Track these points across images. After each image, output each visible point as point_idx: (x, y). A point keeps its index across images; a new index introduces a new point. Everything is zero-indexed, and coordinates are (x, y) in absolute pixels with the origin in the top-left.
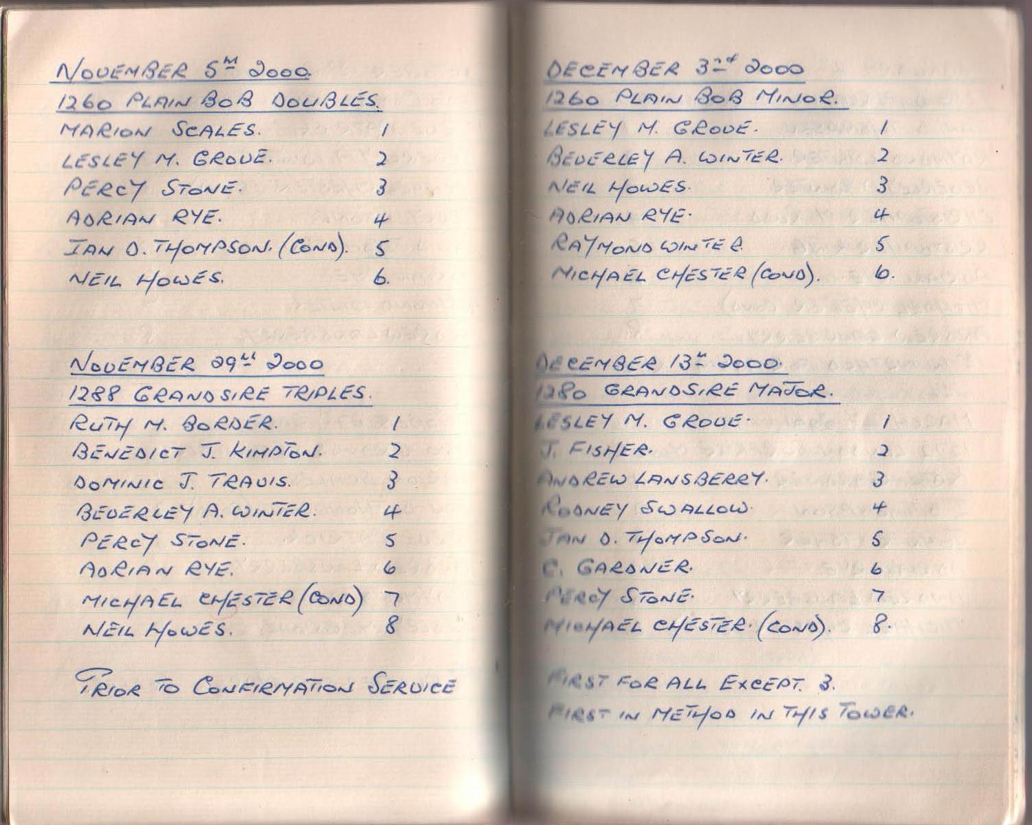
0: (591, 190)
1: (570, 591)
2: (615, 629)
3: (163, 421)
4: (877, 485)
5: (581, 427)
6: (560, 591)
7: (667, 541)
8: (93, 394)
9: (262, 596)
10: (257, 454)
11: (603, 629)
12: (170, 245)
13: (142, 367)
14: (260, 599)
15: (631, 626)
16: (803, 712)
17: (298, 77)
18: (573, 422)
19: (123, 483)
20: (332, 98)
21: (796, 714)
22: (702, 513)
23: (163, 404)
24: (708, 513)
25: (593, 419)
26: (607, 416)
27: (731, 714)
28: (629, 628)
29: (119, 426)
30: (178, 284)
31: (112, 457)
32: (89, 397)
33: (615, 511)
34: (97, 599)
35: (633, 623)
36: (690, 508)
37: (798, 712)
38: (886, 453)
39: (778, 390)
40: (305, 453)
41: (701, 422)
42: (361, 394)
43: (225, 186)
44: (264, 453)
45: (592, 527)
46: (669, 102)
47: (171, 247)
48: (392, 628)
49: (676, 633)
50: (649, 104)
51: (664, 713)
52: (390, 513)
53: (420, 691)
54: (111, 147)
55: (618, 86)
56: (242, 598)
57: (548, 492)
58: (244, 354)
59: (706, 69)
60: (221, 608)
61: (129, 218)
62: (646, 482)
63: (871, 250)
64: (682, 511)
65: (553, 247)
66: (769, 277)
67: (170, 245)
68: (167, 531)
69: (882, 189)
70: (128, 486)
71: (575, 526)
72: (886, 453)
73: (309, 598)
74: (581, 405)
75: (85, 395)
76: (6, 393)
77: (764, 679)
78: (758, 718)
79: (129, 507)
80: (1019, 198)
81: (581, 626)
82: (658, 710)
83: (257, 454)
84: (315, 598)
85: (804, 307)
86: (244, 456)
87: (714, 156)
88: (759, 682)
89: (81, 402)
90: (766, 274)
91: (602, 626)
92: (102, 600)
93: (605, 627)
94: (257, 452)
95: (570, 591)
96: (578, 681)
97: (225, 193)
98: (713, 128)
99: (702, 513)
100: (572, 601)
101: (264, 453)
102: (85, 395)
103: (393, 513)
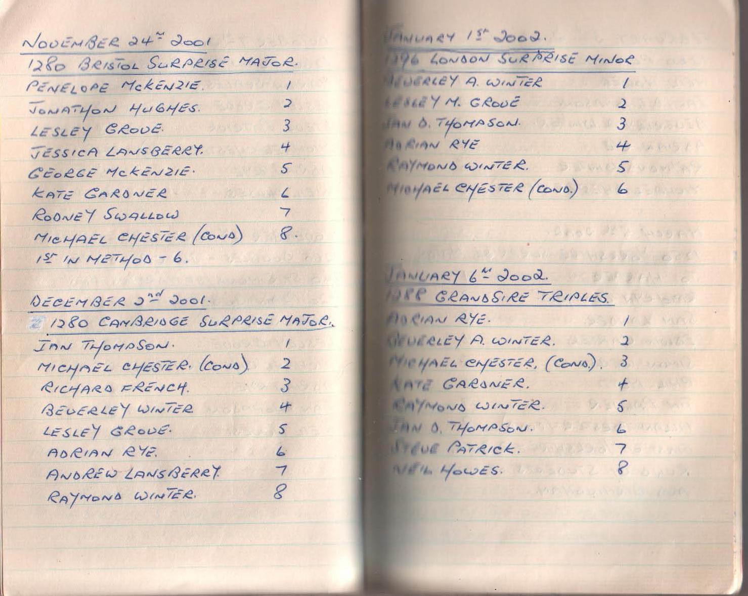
0: (34, 133)
7: (464, 125)
9: (511, 361)
11: (424, 191)
12: (460, 426)
16: (99, 346)
17: (472, 283)
18: (60, 132)
20: (87, 62)
21: (122, 260)
22: (154, 218)
23: (455, 303)
27: (108, 389)
30: (491, 86)
31: (153, 476)
33: (454, 342)
34: (48, 366)
36: (142, 474)
40: (131, 152)
41: (93, 498)
42: (623, 168)
43: (504, 383)
45: (440, 375)
50: (464, 302)
51: (95, 260)
52: (621, 146)
54: (68, 100)
56: (499, 361)
57: (395, 396)
58: (485, 268)
59: (624, 125)
60: (139, 372)
62: (133, 477)
63: (614, 409)
66: (544, 191)
67: (460, 426)
68: (109, 424)
69: (286, 128)
71: (415, 374)
73: (41, 301)
79: (497, 359)
80: (736, 188)
81: (409, 189)
82: (284, 317)
84: (206, 236)
85: (598, 405)
90: (542, 189)
91: (423, 189)
92: (52, 366)
93: (425, 189)
96: (412, 143)
97: (521, 409)
98: (57, 174)
99: (154, 218)
100: (421, 84)
103: (624, 146)
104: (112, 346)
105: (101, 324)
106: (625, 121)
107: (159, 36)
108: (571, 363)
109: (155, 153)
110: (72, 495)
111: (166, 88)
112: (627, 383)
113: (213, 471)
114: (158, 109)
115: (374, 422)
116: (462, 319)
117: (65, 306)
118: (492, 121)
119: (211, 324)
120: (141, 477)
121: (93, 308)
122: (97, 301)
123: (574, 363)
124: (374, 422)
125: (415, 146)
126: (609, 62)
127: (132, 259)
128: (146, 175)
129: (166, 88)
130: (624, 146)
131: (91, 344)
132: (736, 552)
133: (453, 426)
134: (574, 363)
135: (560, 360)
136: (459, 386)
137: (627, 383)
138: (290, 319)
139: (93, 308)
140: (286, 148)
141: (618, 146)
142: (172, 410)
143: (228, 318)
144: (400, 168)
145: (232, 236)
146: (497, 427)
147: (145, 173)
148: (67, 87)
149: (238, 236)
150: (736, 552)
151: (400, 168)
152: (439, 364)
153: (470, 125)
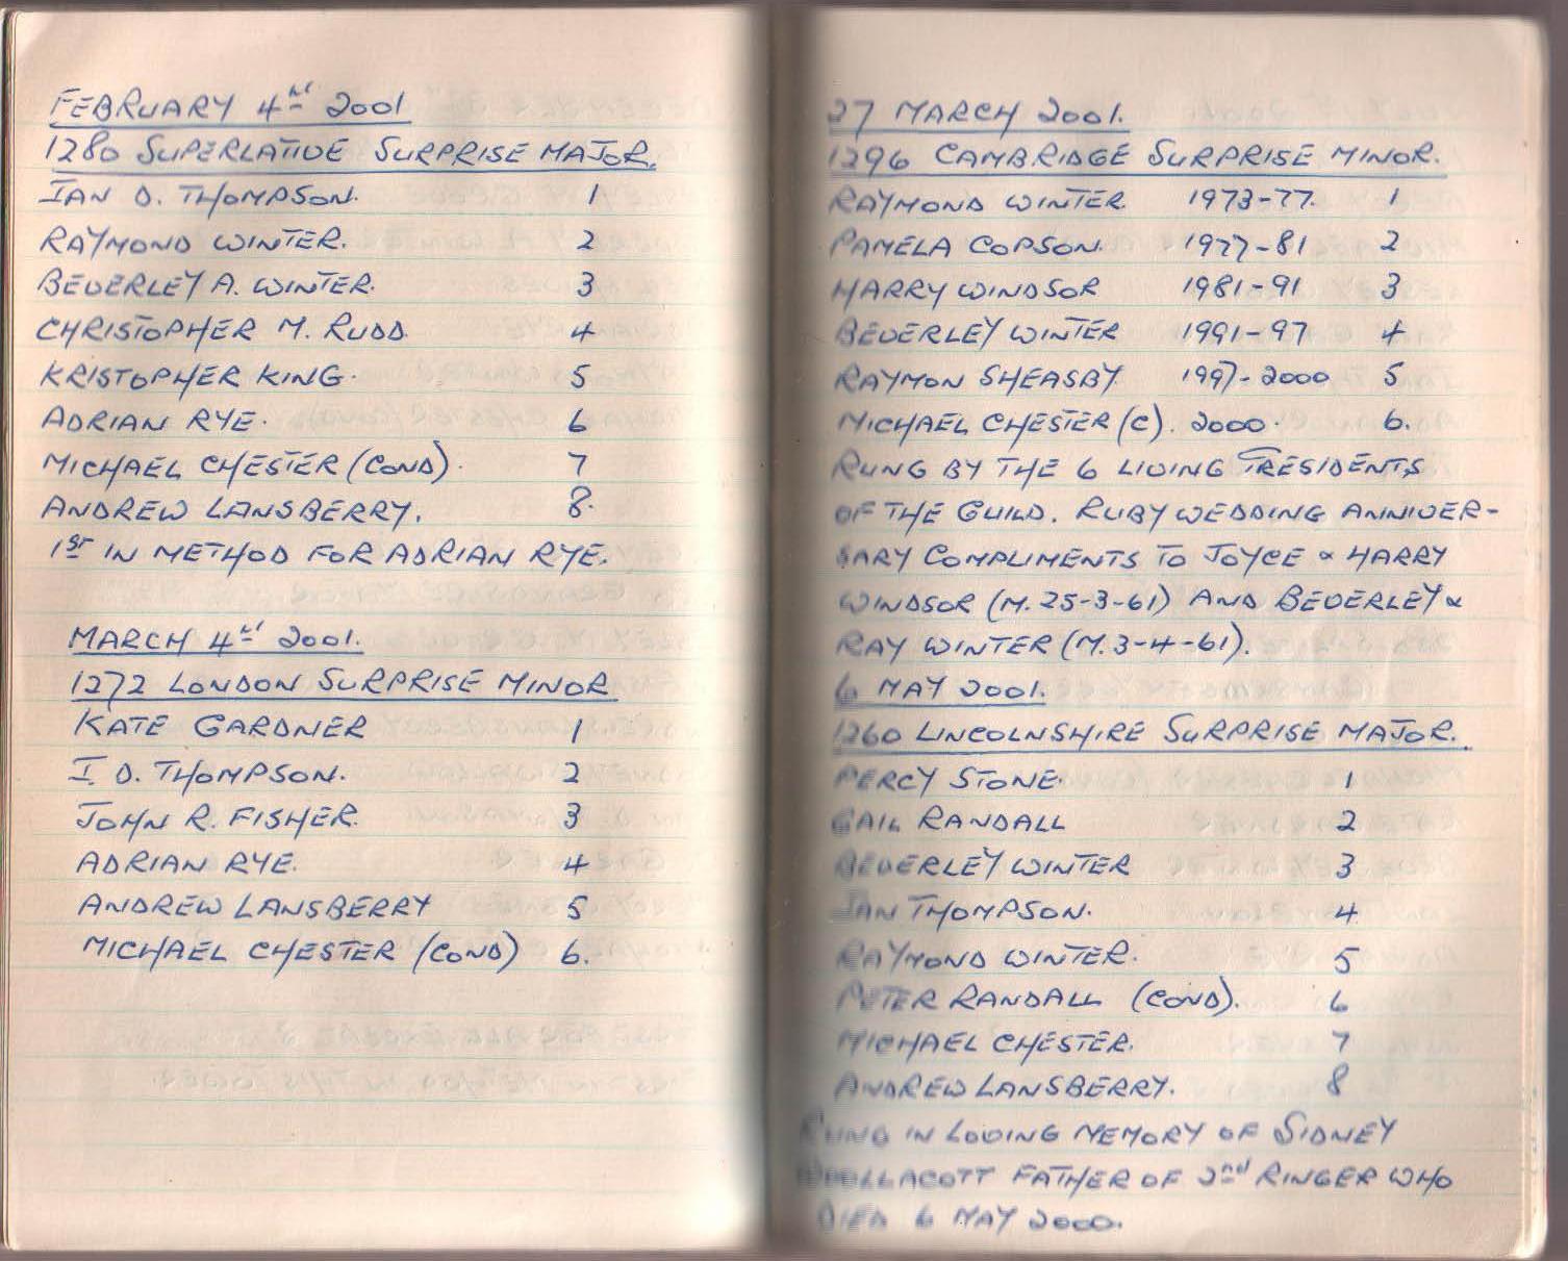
1: (869, 858)
2: (142, 472)
3: (1025, 599)
4: (584, 293)
5: (957, 1140)
6: (861, 990)
8: (380, 462)
10: (1009, 605)
12: (906, 509)
13: (515, 685)
14: (187, 196)
15: (210, 953)
19: (881, 825)
24: (948, 340)
25: (973, 862)
26: (976, 464)
28: (910, 249)
29: (200, 199)
32: (77, 156)
35: (213, 948)
37: (57, 425)
38: (97, 116)
39: (1057, 994)
44: (1052, 561)
46: (300, 291)
47: (1007, 376)
48: (1207, 199)
49: (1027, 1055)
53: (1164, 472)
55: (90, 130)
57: (837, 223)
61: (174, 948)
64: (1000, 383)
65: (838, 962)
70: (999, 296)
72: (97, 116)
74: (896, 753)
75: (70, 152)
76: (10, 96)
77: (476, 946)
78: (296, 291)
83: (1009, 605)
86: (104, 732)
87: (1381, 471)
88: (986, 107)
89: (137, 696)
94: (1043, 557)
95: (875, 994)
101: (1052, 561)
102: (70, 152)
104: (216, 775)
105: (988, 427)
106: (1351, 862)
107: (295, 100)
108: (397, 466)
109: (310, 515)
110: (1154, 509)
111: (319, 778)
112: (1353, 829)
113: (1105, 377)
114: (1082, 473)
115: (786, 903)
116: (1102, 1135)
117: (1113, 163)
118: (281, 771)
119: (1173, 161)
120: (121, 732)
121: (1012, 169)
122: (311, 509)
123: (403, 466)
124: (786, 903)
125: (861, 961)
126: (1010, 1003)
127: (1028, 424)
128: (1450, 518)
129: (319, 778)
130: (578, 866)
131: (174, 769)
132: (1535, 1173)
133: (1006, 467)
134: (403, 466)
135: (379, 459)
136: (1005, 913)
137: (1353, 829)
138: (65, 461)
139: (1012, 169)
140: (574, 870)
141: (574, 335)
142: (295, 241)
143: (379, 675)
144: (865, 963)
145: (140, 907)
146: (266, 770)
147: (1445, 514)
148: (1371, 1133)
149: (507, 948)
150: (1535, 1173)
151: (865, 963)
152: (143, 468)
153: (907, 208)
